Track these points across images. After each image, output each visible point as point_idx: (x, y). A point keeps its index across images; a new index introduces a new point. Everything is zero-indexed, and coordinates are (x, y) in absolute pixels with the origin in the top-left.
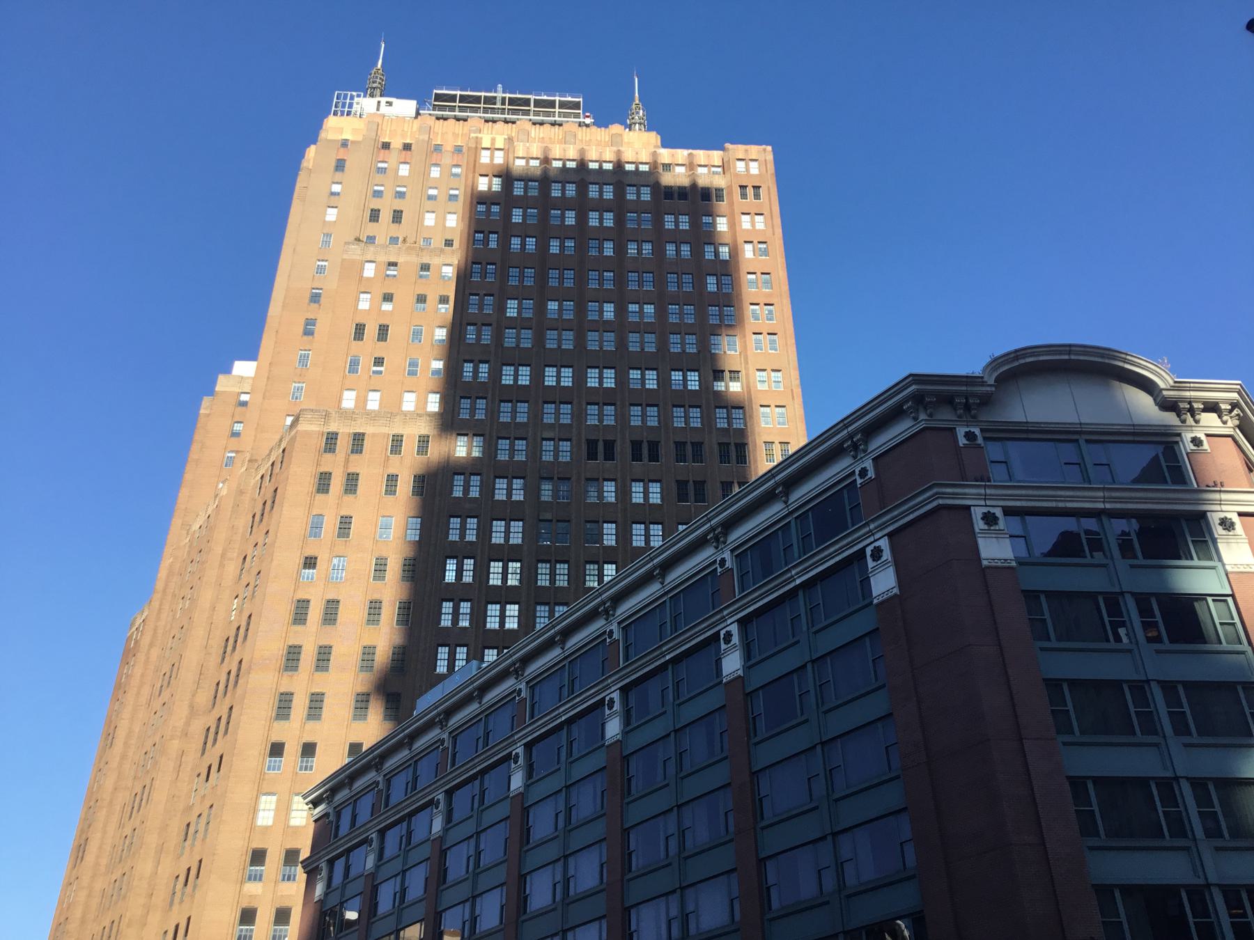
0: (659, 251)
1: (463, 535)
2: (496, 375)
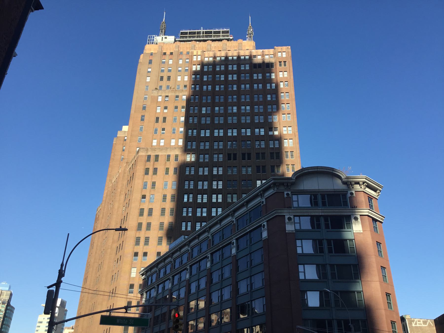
0: (252, 87)
1: (189, 186)
2: (199, 133)
